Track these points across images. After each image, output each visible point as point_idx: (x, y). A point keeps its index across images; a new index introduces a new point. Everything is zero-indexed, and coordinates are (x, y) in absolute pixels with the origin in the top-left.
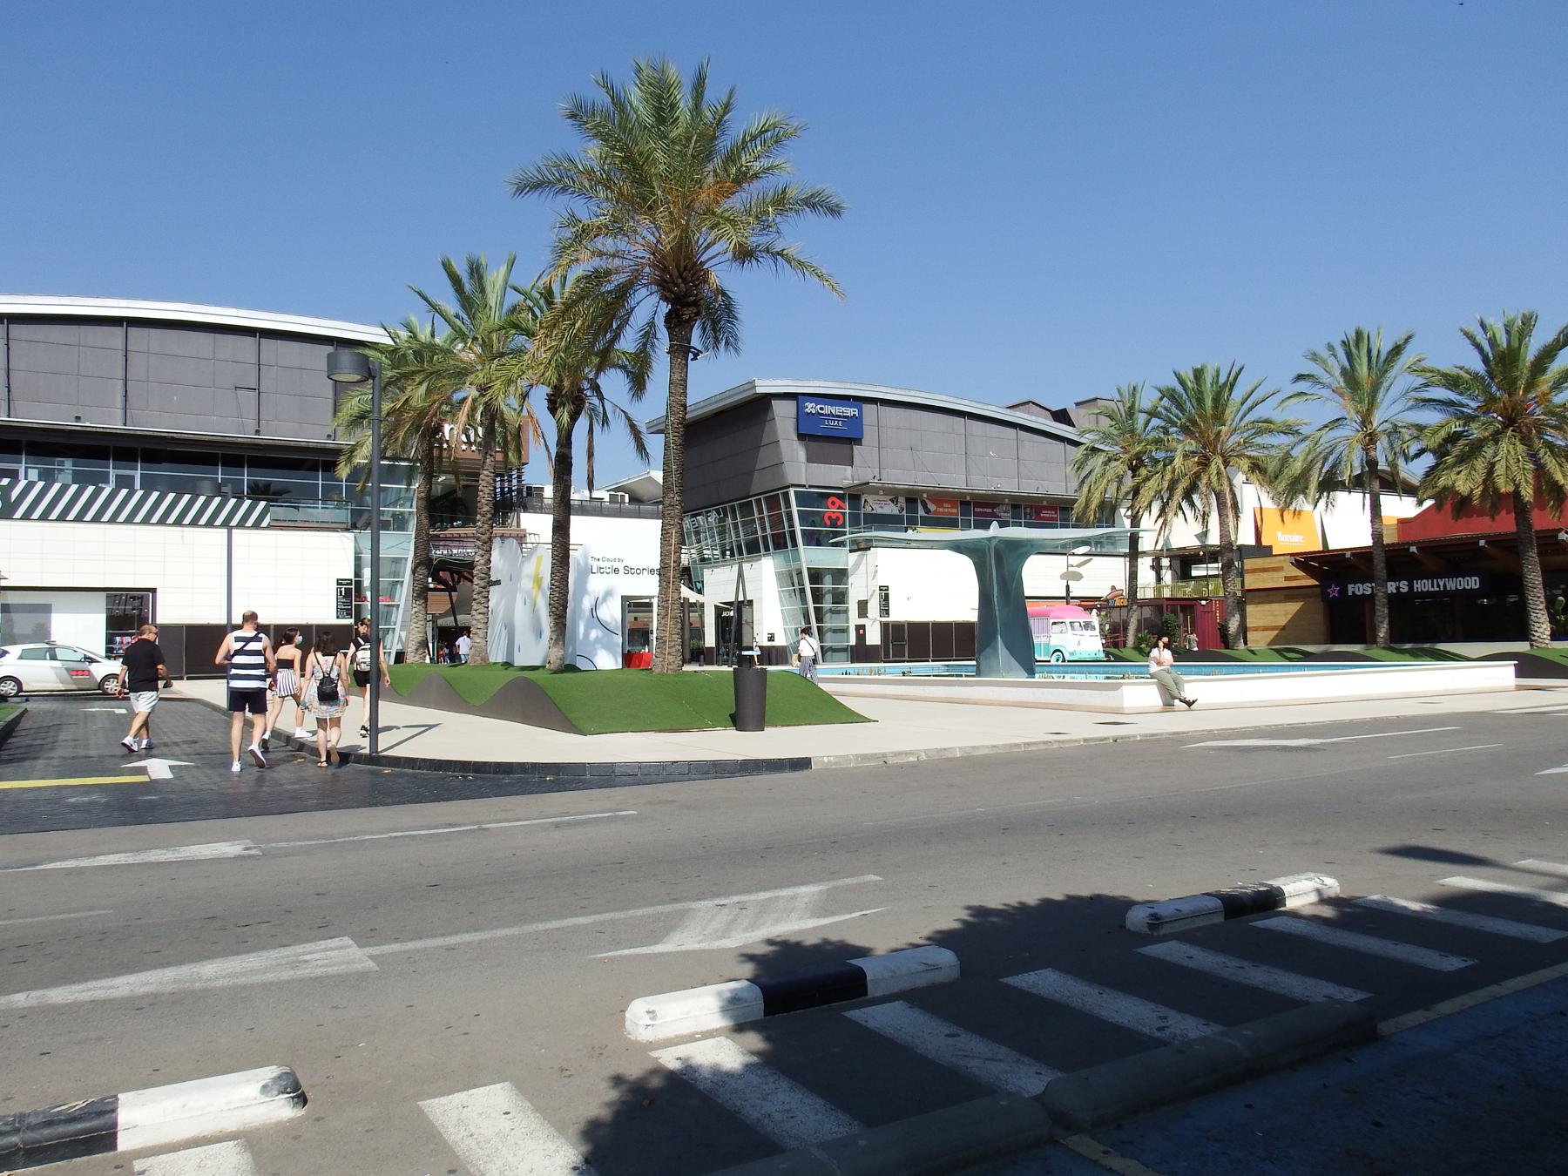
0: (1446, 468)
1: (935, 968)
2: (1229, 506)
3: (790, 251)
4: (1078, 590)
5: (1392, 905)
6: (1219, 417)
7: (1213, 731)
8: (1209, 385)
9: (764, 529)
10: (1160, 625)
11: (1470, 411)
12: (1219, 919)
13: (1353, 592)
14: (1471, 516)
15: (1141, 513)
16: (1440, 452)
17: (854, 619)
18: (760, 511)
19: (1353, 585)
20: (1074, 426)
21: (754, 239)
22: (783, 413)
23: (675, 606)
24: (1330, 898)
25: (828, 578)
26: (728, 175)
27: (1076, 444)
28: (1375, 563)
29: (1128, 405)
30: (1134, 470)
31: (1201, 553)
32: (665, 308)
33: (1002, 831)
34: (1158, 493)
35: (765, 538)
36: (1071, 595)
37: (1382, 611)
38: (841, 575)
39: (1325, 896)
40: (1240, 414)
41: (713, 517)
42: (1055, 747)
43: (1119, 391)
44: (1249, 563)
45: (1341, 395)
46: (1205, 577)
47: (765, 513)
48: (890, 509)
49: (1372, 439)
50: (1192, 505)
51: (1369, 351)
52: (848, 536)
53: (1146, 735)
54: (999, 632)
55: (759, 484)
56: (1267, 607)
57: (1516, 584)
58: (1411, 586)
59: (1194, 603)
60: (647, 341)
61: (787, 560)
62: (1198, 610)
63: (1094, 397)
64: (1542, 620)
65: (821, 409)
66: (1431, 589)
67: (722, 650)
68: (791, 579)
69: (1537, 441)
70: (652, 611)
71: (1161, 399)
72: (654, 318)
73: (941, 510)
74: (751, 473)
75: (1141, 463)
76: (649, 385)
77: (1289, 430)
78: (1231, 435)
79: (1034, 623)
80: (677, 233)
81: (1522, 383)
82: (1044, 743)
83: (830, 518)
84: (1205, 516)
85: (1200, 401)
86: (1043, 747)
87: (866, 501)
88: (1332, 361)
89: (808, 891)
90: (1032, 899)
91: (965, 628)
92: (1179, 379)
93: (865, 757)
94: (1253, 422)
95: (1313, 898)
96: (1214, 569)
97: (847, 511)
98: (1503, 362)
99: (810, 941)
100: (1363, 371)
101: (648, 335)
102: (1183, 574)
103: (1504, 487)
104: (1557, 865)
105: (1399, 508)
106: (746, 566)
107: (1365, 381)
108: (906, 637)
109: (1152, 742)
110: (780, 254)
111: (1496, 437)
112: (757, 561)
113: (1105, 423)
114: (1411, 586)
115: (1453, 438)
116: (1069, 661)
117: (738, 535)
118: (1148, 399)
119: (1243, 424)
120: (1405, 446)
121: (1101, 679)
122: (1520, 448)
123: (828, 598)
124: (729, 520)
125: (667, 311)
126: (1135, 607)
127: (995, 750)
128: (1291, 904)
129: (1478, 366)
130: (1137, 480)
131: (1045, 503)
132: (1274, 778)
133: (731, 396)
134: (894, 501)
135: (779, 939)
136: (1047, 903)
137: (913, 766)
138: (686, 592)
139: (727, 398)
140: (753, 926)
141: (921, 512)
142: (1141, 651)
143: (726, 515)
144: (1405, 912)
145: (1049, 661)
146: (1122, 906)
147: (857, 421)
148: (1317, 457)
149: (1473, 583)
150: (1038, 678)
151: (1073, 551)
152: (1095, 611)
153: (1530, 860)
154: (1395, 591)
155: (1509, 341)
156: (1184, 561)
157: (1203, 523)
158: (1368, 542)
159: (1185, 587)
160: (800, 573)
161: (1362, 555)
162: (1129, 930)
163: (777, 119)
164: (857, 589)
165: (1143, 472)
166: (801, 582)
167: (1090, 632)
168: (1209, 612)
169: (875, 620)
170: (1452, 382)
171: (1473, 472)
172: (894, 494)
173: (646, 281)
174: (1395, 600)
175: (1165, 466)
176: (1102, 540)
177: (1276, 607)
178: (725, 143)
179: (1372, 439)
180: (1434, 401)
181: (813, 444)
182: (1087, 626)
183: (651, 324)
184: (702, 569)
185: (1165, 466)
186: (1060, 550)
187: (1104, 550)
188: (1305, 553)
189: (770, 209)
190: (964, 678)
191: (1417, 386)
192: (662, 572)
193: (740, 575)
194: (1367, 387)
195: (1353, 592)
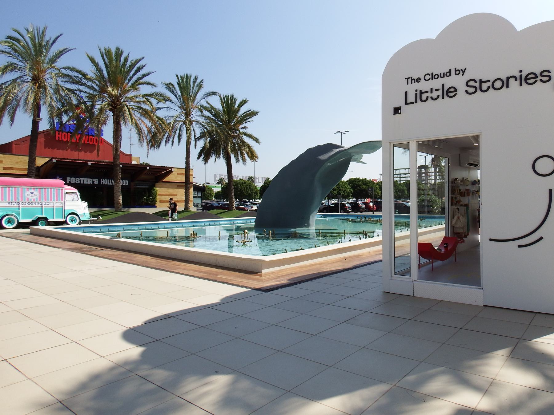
14: (54, 149)
19: (70, 178)
58: (99, 182)
66: (108, 184)
114: (99, 182)
154: (92, 183)
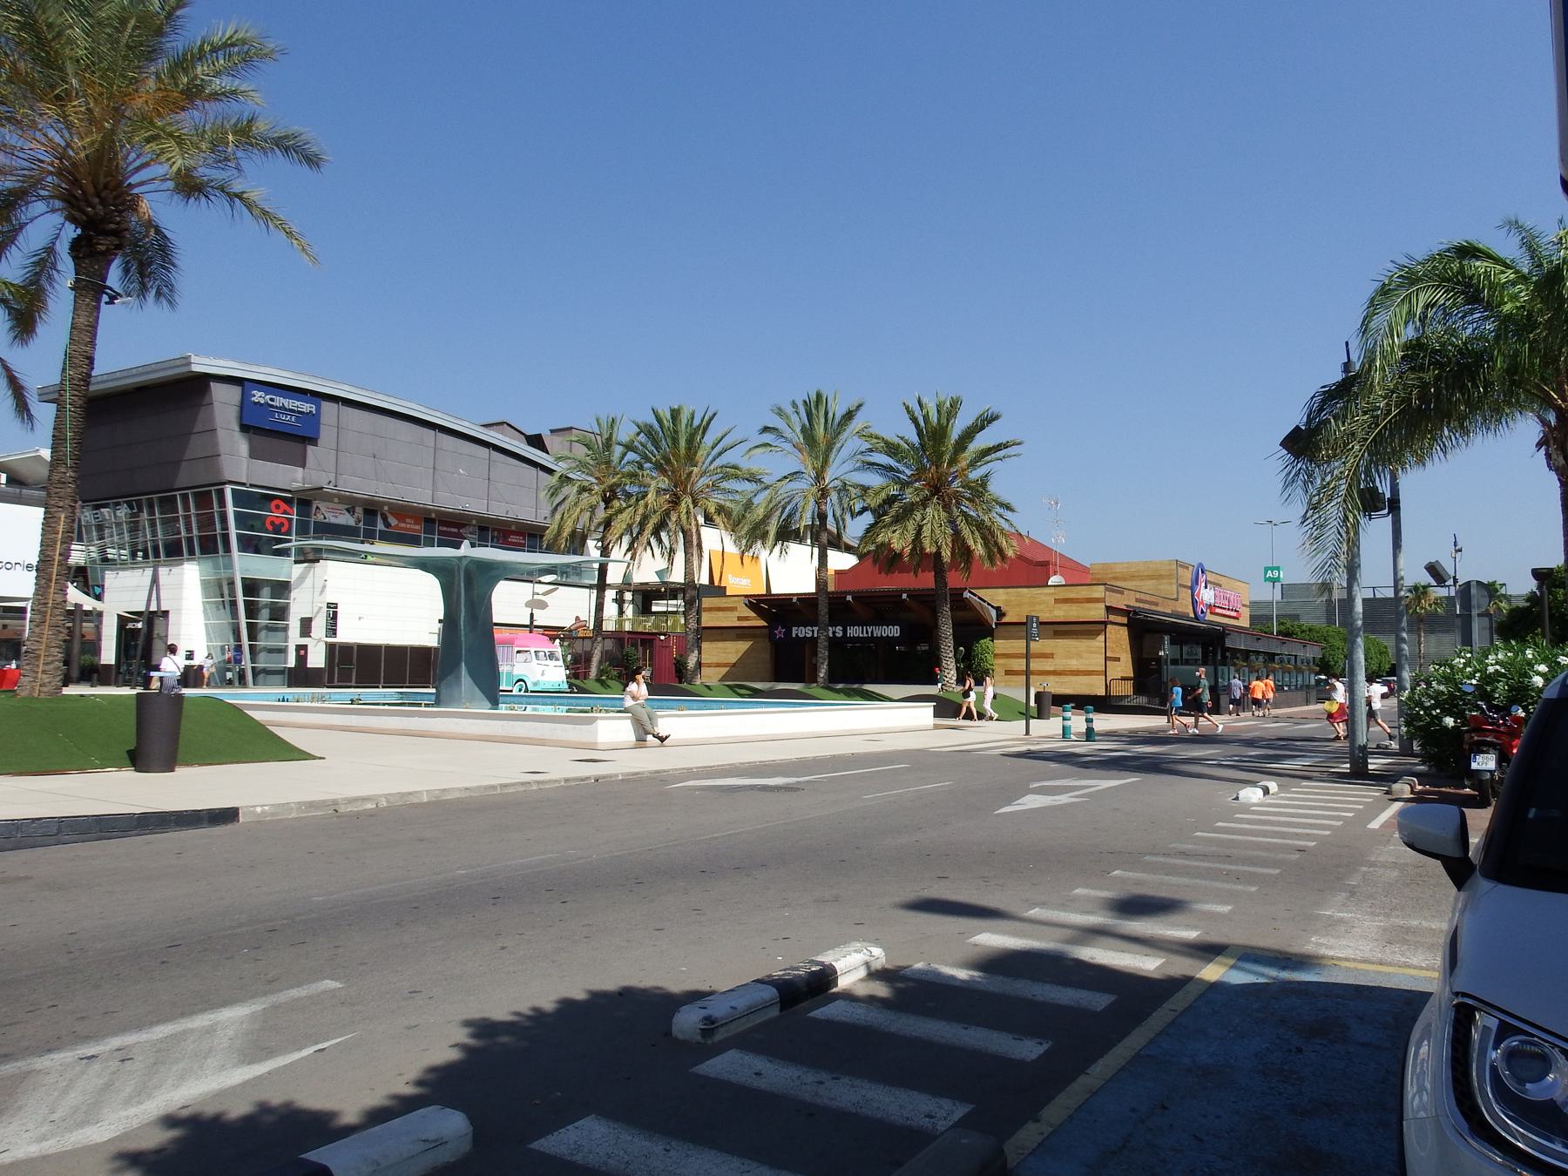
0: (884, 527)
1: (440, 1143)
2: (693, 546)
3: (253, 195)
4: (542, 618)
5: (939, 974)
6: (691, 458)
7: (692, 769)
8: (683, 426)
9: (189, 529)
10: (620, 657)
11: (905, 478)
12: (774, 1012)
13: (797, 634)
15: (611, 545)
16: (879, 513)
17: (294, 637)
18: (187, 508)
19: (796, 628)
20: (548, 453)
21: (207, 171)
22: (224, 400)
23: (57, 612)
24: (877, 971)
25: (266, 591)
26: (177, 85)
27: (550, 471)
28: (820, 609)
29: (606, 436)
30: (607, 501)
31: (663, 589)
32: (71, 232)
33: (492, 901)
34: (629, 528)
35: (190, 541)
36: (535, 623)
37: (823, 653)
38: (282, 588)
39: (873, 968)
40: (710, 458)
41: (123, 512)
42: (534, 788)
43: (598, 420)
44: (707, 602)
45: (800, 450)
46: (665, 612)
47: (193, 511)
48: (346, 519)
49: (824, 493)
50: (660, 541)
51: (826, 414)
52: (294, 543)
53: (628, 774)
54: (463, 658)
55: (185, 477)
56: (721, 644)
57: (929, 633)
58: (845, 631)
59: (654, 637)
60: (42, 270)
61: (216, 567)
62: (657, 643)
63: (569, 426)
64: (951, 667)
65: (272, 400)
66: (861, 635)
67: (123, 668)
68: (220, 591)
69: (955, 510)
70: (25, 619)
71: (638, 434)
72: (54, 244)
73: (403, 525)
74: (179, 462)
75: (614, 496)
76: (40, 329)
77: (752, 478)
78: (701, 477)
79: (501, 652)
80: (97, 137)
81: (947, 457)
82: (523, 784)
83: (272, 523)
84: (672, 551)
85: (675, 441)
86: (522, 789)
87: (317, 508)
88: (794, 418)
89: (234, 1015)
90: (548, 1004)
91: (422, 653)
92: (656, 416)
93: (311, 805)
94: (722, 467)
95: (862, 973)
96: (676, 604)
97: (295, 517)
98: (932, 435)
99: (238, 1109)
100: (820, 431)
101: (44, 263)
102: (644, 609)
103: (930, 548)
104: (1062, 914)
105: (840, 561)
106: (163, 571)
107: (821, 440)
108: (355, 661)
109: (634, 781)
110: (239, 196)
111: (924, 503)
112: (178, 565)
113: (581, 451)
114: (845, 631)
115: (890, 501)
116: (532, 692)
117: (154, 533)
118: (625, 433)
119: (712, 467)
120: (852, 503)
121: (561, 711)
122: (943, 514)
123: (265, 613)
124: (145, 515)
125: (76, 236)
126: (599, 639)
127: (467, 794)
128: (844, 983)
129: (915, 439)
130: (610, 512)
131: (513, 528)
132: (767, 822)
133: (158, 371)
134: (351, 511)
135: (185, 1113)
136: (567, 1005)
137: (371, 814)
138: (74, 595)
139: (148, 373)
140: (142, 1092)
141: (380, 526)
142: (603, 683)
143: (140, 510)
144: (952, 983)
145: (511, 691)
146: (661, 1005)
147: (314, 419)
148: (776, 505)
149: (894, 631)
150: (503, 709)
151: (540, 579)
152: (558, 641)
153: (1037, 909)
155: (939, 420)
156: (646, 596)
157: (669, 559)
158: (810, 587)
159: (646, 621)
160: (231, 583)
161: (804, 599)
162: (676, 1038)
163: (249, 35)
164: (300, 605)
165: (616, 504)
166: (232, 593)
167: (554, 663)
168: (667, 647)
169: (319, 640)
170: (892, 449)
171: (905, 532)
172: (350, 503)
173: (46, 193)
174: (834, 643)
175: (637, 500)
176: (568, 570)
177: (728, 644)
178: (175, 45)
179: (824, 493)
180: (878, 465)
181: (258, 439)
182: (551, 656)
183: (50, 250)
184: (103, 571)
185: (637, 500)
186: (525, 578)
187: (570, 581)
188: (758, 595)
189: (230, 137)
190: (423, 709)
191: (864, 450)
192: (43, 568)
193: (155, 580)
194: (823, 446)
195: (797, 634)
